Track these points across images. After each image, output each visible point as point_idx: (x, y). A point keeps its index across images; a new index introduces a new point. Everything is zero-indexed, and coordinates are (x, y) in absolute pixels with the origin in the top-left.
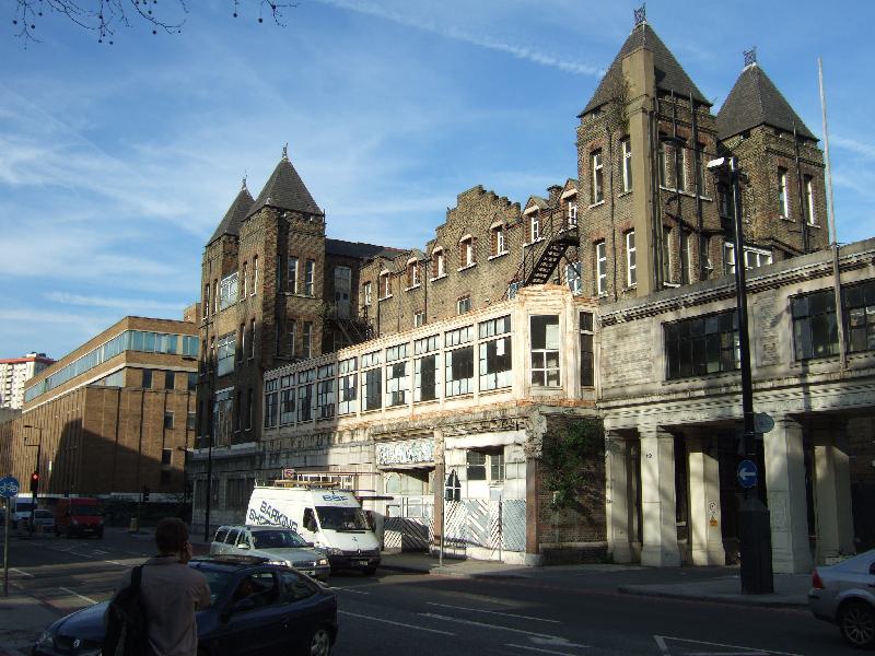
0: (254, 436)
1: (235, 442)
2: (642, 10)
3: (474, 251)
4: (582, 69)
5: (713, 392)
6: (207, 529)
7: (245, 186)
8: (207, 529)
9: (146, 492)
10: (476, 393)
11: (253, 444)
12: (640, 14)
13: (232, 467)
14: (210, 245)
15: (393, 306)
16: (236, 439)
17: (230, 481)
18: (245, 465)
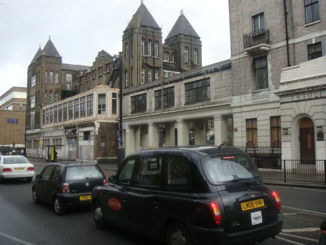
0: (38, 127)
1: (36, 129)
2: (182, 10)
3: (295, 215)
4: (168, 170)
5: (308, 176)
6: (60, 146)
7: (50, 38)
8: (60, 146)
9: (14, 144)
10: (33, 141)
11: (39, 130)
12: (182, 11)
13: (34, 136)
14: (38, 59)
15: (82, 86)
16: (36, 128)
17: (34, 140)
18: (37, 136)
